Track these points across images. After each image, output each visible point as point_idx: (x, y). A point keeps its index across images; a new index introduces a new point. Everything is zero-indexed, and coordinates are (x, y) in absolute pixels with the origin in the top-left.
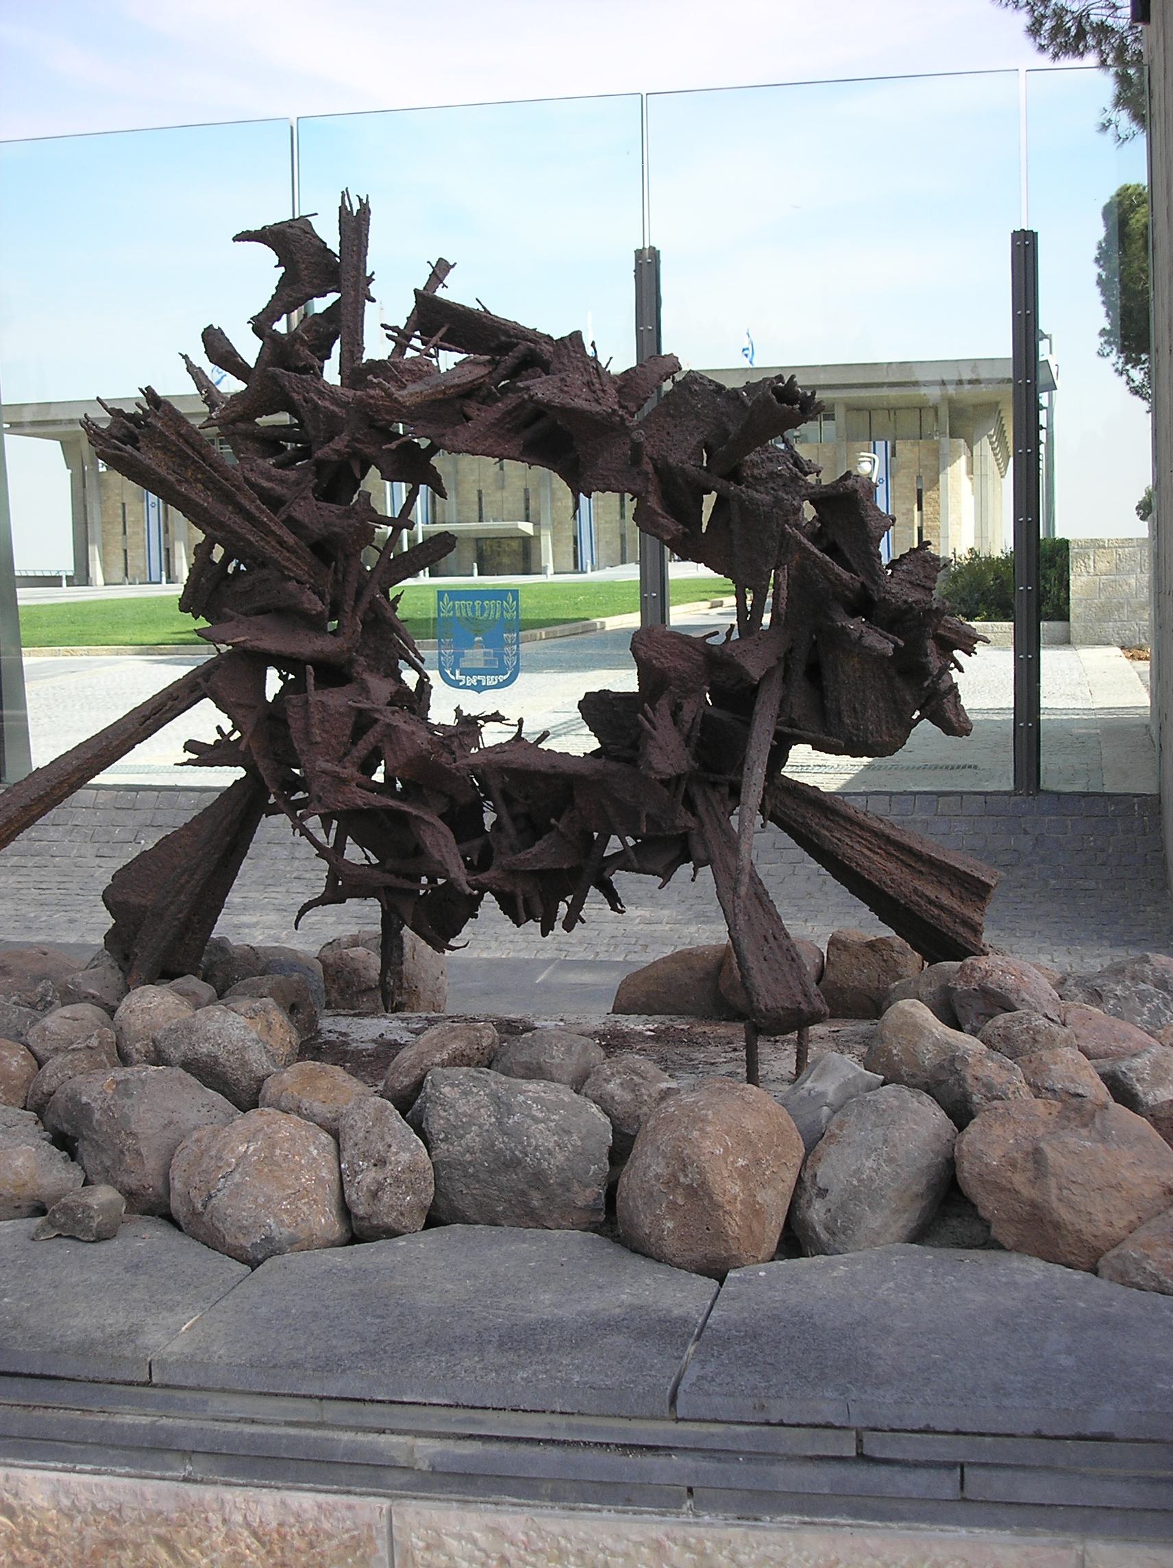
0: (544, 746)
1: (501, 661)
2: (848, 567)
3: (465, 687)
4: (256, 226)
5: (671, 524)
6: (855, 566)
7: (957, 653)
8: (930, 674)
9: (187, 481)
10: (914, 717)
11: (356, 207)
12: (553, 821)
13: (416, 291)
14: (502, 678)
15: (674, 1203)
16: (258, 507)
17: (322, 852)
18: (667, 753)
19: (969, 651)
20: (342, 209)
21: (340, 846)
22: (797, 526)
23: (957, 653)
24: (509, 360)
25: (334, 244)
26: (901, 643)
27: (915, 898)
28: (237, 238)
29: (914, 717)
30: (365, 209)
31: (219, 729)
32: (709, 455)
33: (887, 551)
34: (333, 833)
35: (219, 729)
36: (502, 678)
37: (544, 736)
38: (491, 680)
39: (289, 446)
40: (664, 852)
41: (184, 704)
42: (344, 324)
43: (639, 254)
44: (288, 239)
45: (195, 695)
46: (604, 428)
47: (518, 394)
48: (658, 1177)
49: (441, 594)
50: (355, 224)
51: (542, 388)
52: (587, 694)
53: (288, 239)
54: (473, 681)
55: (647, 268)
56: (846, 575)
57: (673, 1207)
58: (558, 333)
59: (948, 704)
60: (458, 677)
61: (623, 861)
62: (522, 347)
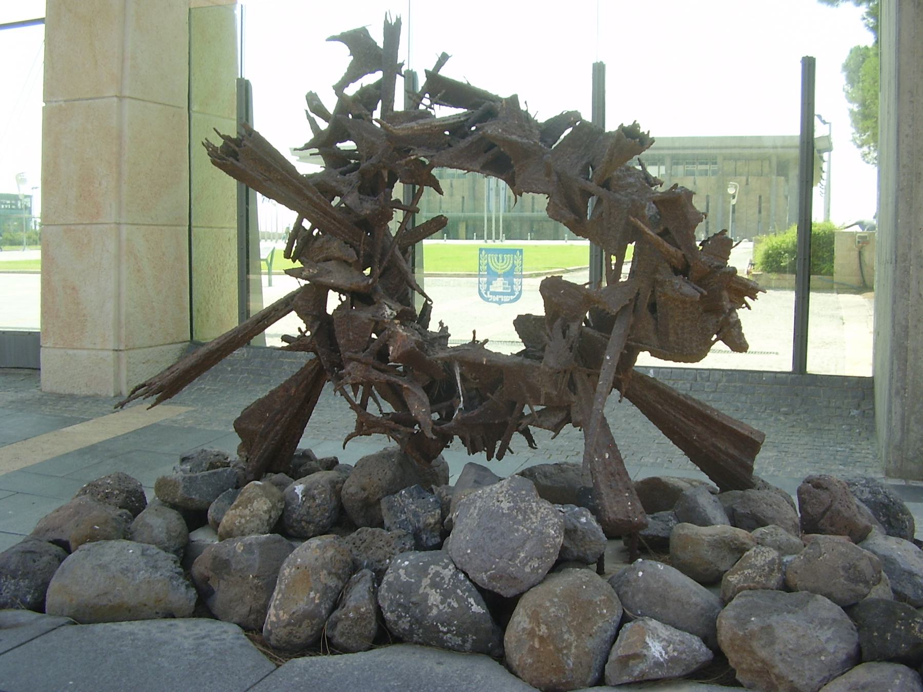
0: (486, 346)
1: (512, 288)
2: (674, 243)
3: (492, 301)
4: (337, 33)
5: (571, 215)
6: (679, 242)
7: (747, 299)
8: (724, 312)
9: (270, 180)
10: (713, 339)
11: (394, 21)
12: (489, 394)
13: (426, 71)
14: (512, 297)
15: (532, 647)
16: (318, 197)
17: (354, 407)
18: (557, 355)
19: (753, 298)
20: (386, 22)
21: (364, 405)
22: (642, 218)
23: (747, 299)
24: (478, 112)
25: (380, 44)
26: (705, 293)
27: (711, 449)
28: (328, 40)
29: (713, 339)
30: (399, 21)
31: (300, 330)
32: (581, 171)
33: (701, 235)
34: (360, 395)
35: (300, 330)
36: (512, 297)
37: (486, 341)
38: (507, 298)
39: (353, 161)
40: (560, 414)
41: (280, 315)
42: (383, 91)
43: (594, 65)
44: (357, 41)
45: (288, 309)
46: (526, 153)
47: (492, 137)
48: (524, 629)
49: (481, 250)
50: (392, 32)
51: (492, 129)
52: (519, 316)
53: (357, 41)
54: (497, 298)
55: (599, 71)
56: (672, 249)
57: (532, 649)
58: (504, 94)
59: (734, 332)
60: (489, 296)
61: (536, 419)
62: (487, 104)
